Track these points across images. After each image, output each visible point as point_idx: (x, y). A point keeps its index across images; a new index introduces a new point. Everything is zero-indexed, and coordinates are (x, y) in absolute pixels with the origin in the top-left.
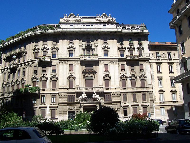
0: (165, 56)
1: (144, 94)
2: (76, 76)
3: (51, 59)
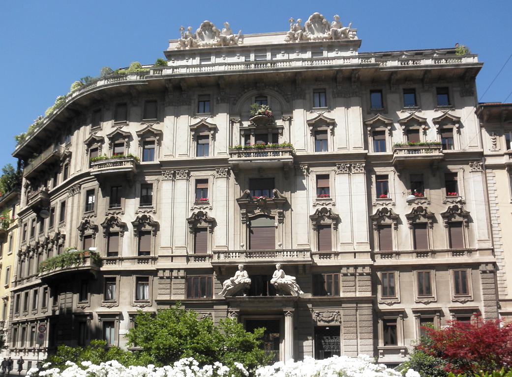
1: (460, 272)
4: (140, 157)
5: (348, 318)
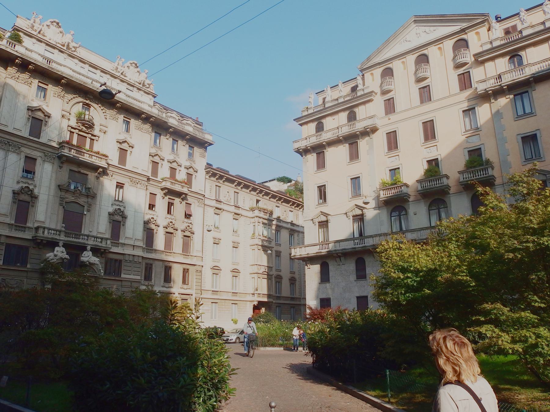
0: (229, 199)
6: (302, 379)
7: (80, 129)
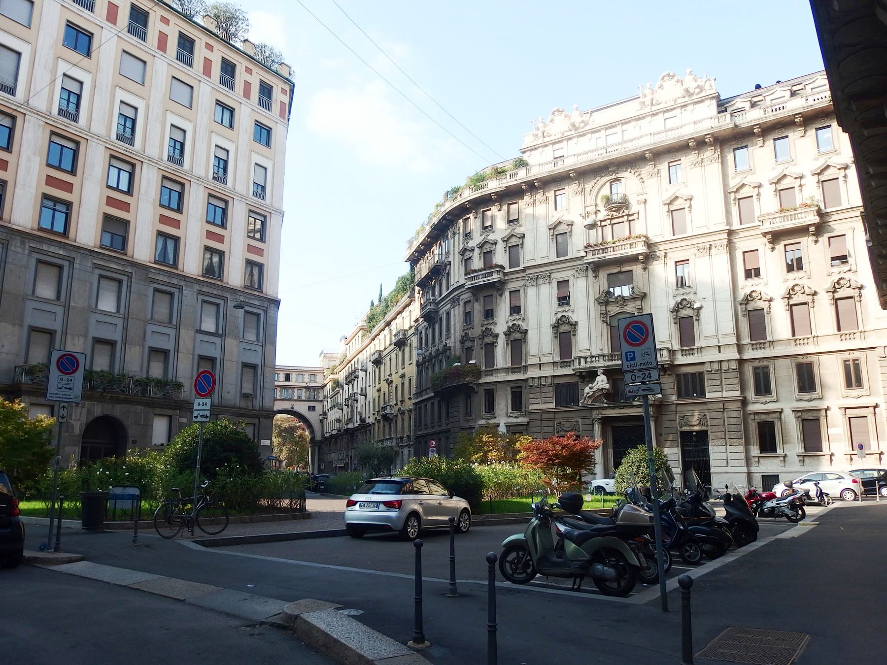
2: (578, 318)
3: (505, 274)
4: (506, 264)
5: (714, 422)
6: (86, 534)
7: (610, 217)
